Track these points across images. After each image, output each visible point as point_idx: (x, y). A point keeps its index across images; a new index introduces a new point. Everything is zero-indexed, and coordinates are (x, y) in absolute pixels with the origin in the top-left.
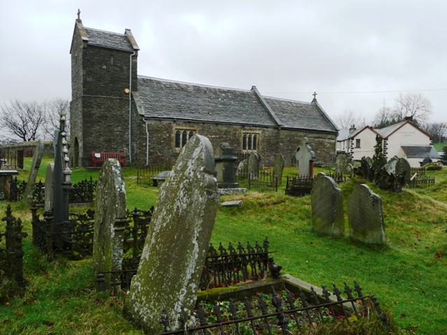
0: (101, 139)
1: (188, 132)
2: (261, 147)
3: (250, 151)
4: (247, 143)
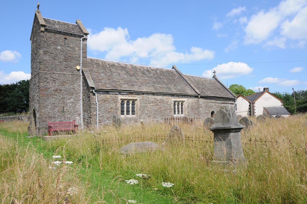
0: (56, 110)
1: (131, 102)
2: (187, 112)
3: (179, 115)
4: (115, 93)
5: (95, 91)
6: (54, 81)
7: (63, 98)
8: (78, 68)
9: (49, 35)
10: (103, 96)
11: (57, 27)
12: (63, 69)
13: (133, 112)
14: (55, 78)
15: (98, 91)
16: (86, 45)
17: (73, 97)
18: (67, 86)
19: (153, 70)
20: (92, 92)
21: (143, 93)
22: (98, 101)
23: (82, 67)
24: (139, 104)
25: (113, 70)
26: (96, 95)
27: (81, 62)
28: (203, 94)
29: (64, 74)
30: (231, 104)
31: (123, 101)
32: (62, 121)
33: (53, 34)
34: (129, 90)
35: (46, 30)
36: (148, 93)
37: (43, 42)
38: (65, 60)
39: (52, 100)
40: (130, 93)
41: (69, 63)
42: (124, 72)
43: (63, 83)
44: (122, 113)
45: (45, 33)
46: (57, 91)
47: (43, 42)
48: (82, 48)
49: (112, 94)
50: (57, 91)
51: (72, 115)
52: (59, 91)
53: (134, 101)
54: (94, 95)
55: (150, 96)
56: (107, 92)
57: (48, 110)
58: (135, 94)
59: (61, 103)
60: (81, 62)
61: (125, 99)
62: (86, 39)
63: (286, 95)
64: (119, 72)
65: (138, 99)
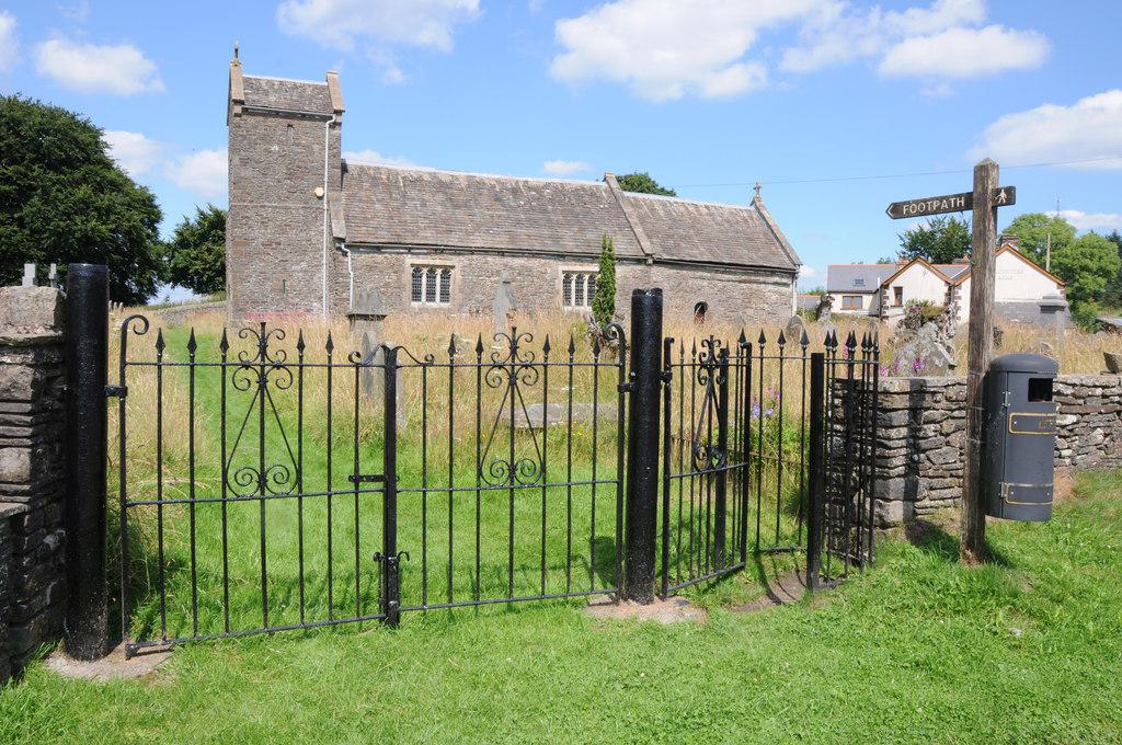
1: (439, 271)
5: (347, 246)
8: (319, 192)
9: (251, 120)
10: (365, 258)
11: (272, 98)
13: (445, 296)
15: (354, 246)
16: (339, 138)
17: (307, 258)
18: (292, 234)
19: (531, 189)
20: (339, 249)
21: (472, 252)
22: (354, 269)
23: (328, 190)
24: (459, 277)
25: (412, 193)
26: (349, 254)
27: (326, 179)
28: (668, 254)
29: (286, 208)
30: (775, 283)
31: (417, 269)
33: (261, 118)
34: (434, 243)
35: (245, 110)
36: (486, 251)
37: (240, 139)
38: (290, 176)
39: (258, 265)
40: (436, 250)
41: (298, 182)
42: (440, 197)
43: (283, 229)
44: (416, 295)
45: (244, 117)
47: (240, 139)
48: (330, 146)
49: (390, 253)
53: (446, 271)
54: (345, 254)
55: (490, 259)
56: (377, 248)
57: (250, 285)
58: (450, 254)
59: (280, 272)
60: (326, 179)
61: (424, 266)
62: (340, 124)
64: (426, 197)
65: (456, 264)
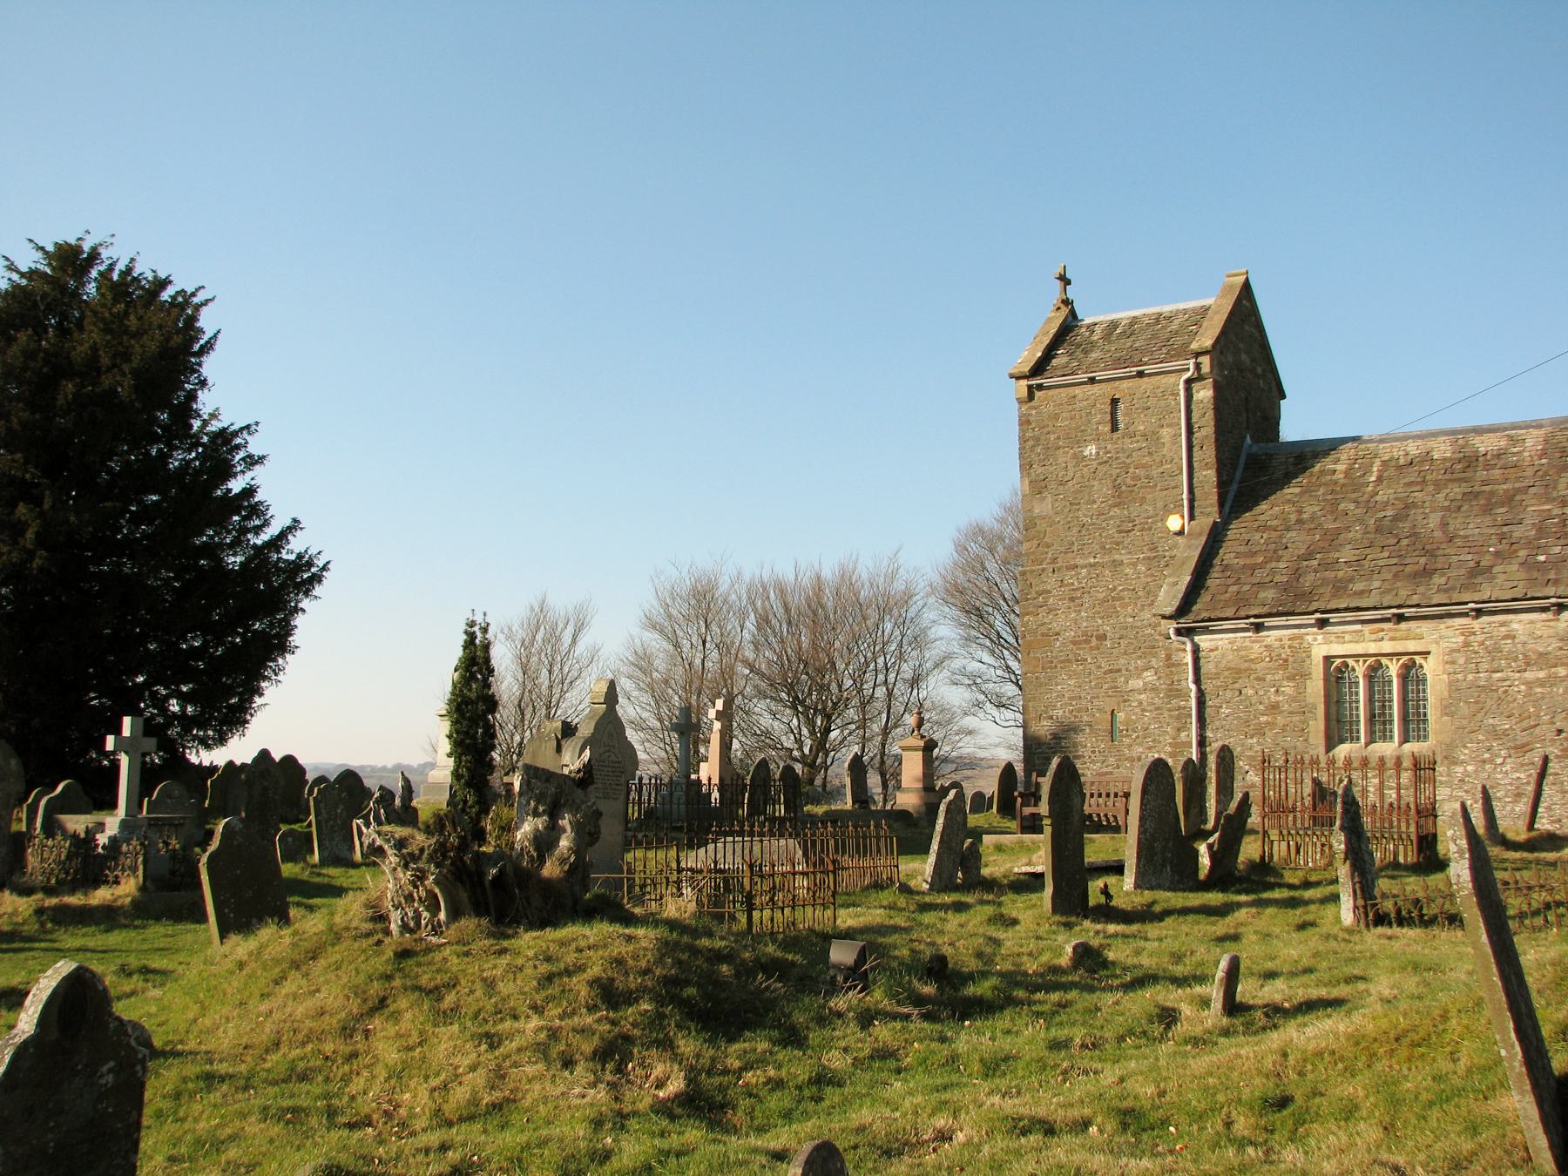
6: (1072, 599)
7: (1111, 671)
12: (1111, 543)
14: (1077, 589)
32: (1107, 773)
41: (1135, 509)
46: (1087, 641)
50: (1087, 641)
51: (1150, 748)
52: (1094, 642)
63: (253, 932)
